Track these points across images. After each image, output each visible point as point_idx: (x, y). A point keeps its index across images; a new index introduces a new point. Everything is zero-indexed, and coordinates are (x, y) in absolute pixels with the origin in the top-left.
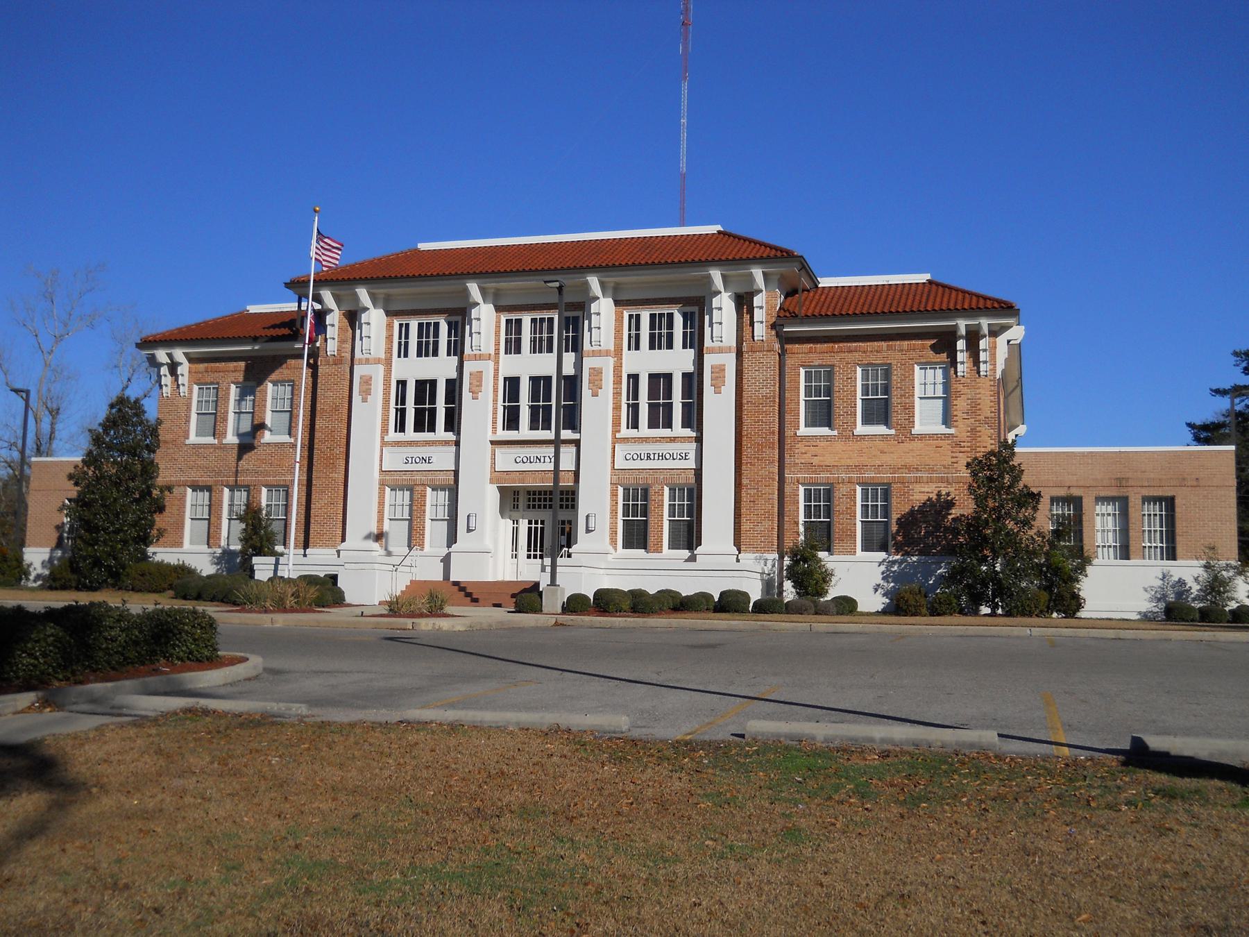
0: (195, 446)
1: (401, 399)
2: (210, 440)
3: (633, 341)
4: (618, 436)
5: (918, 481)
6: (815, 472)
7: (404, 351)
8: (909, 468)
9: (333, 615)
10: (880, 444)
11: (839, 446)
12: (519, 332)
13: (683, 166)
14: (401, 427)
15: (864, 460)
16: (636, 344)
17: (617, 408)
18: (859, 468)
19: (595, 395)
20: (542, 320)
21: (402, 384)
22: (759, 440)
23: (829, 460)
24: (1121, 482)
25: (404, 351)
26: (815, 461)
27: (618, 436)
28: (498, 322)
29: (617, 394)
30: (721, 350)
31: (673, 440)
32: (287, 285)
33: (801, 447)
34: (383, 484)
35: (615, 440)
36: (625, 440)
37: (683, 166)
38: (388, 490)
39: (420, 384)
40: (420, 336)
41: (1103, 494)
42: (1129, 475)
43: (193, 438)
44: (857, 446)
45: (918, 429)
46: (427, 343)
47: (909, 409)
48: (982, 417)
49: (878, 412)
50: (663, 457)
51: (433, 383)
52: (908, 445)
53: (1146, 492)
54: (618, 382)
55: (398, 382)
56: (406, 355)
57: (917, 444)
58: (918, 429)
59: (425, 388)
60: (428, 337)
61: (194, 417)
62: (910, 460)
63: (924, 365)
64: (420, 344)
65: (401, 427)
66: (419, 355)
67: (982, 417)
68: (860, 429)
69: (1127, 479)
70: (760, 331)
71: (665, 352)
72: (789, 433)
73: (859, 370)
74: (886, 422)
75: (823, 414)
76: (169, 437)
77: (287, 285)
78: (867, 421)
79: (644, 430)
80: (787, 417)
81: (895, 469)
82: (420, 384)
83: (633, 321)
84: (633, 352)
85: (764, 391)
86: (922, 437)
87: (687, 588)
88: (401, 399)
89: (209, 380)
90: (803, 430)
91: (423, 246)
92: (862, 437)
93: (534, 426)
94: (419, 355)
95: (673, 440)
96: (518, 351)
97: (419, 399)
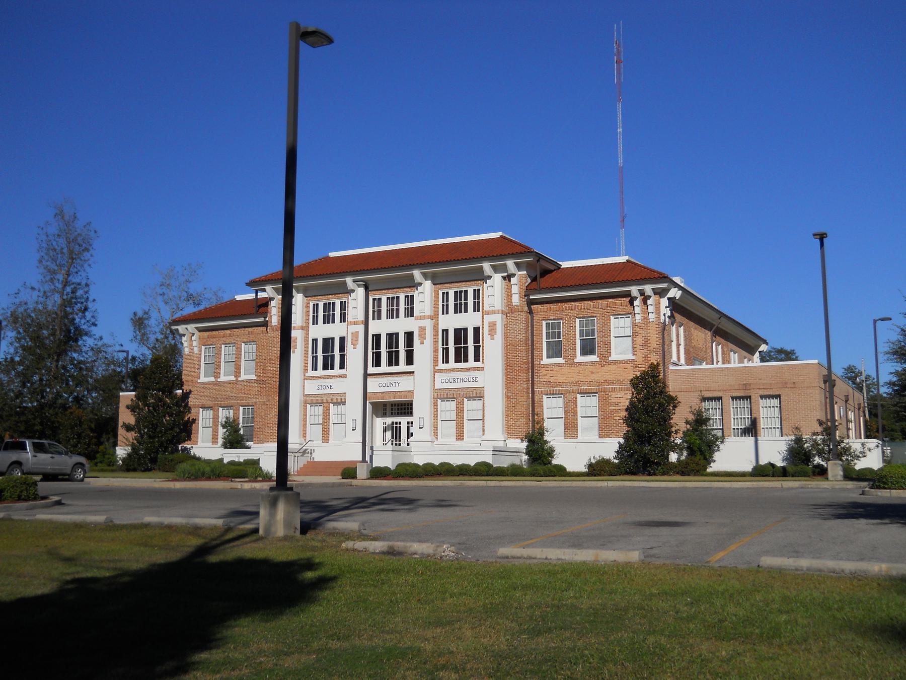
0: (204, 383)
1: (315, 350)
2: (212, 379)
3: (376, 314)
4: (437, 368)
5: (614, 390)
6: (552, 387)
7: (315, 321)
8: (607, 382)
9: (354, 482)
10: (590, 368)
11: (566, 369)
12: (380, 306)
13: (621, 161)
14: (315, 368)
15: (581, 378)
16: (446, 310)
17: (436, 351)
18: (578, 383)
19: (422, 343)
20: (393, 298)
21: (315, 341)
22: (517, 368)
23: (561, 379)
24: (746, 387)
25: (446, 310)
26: (552, 380)
27: (437, 368)
28: (308, 306)
29: (436, 342)
30: (493, 312)
31: (468, 369)
32: (247, 284)
33: (543, 371)
34: (305, 403)
35: (435, 371)
36: (441, 371)
37: (621, 161)
38: (308, 406)
39: (457, 332)
40: (456, 300)
41: (734, 395)
42: (750, 382)
43: (203, 379)
44: (576, 369)
45: (614, 357)
46: (329, 315)
47: (608, 344)
48: (651, 348)
49: (588, 348)
50: (462, 380)
51: (466, 330)
52: (606, 368)
53: (762, 393)
54: (436, 335)
55: (443, 331)
56: (447, 313)
57: (612, 367)
58: (614, 357)
59: (461, 334)
60: (461, 300)
61: (203, 365)
62: (610, 377)
63: (618, 315)
64: (456, 305)
65: (315, 368)
66: (324, 323)
67: (651, 348)
68: (579, 358)
69: (750, 384)
70: (516, 300)
71: (463, 314)
72: (536, 363)
73: (578, 321)
74: (592, 352)
75: (555, 350)
76: (189, 378)
77: (247, 284)
78: (584, 353)
79: (452, 364)
80: (535, 352)
81: (600, 384)
82: (457, 332)
83: (376, 302)
84: (376, 321)
85: (520, 337)
86: (615, 362)
87: (456, 460)
88: (315, 350)
89: (210, 343)
90: (545, 361)
91: (332, 255)
92: (580, 364)
93: (390, 364)
94: (324, 323)
95: (468, 369)
96: (379, 318)
97: (325, 350)
